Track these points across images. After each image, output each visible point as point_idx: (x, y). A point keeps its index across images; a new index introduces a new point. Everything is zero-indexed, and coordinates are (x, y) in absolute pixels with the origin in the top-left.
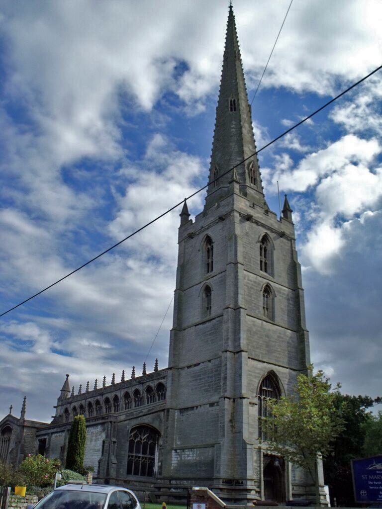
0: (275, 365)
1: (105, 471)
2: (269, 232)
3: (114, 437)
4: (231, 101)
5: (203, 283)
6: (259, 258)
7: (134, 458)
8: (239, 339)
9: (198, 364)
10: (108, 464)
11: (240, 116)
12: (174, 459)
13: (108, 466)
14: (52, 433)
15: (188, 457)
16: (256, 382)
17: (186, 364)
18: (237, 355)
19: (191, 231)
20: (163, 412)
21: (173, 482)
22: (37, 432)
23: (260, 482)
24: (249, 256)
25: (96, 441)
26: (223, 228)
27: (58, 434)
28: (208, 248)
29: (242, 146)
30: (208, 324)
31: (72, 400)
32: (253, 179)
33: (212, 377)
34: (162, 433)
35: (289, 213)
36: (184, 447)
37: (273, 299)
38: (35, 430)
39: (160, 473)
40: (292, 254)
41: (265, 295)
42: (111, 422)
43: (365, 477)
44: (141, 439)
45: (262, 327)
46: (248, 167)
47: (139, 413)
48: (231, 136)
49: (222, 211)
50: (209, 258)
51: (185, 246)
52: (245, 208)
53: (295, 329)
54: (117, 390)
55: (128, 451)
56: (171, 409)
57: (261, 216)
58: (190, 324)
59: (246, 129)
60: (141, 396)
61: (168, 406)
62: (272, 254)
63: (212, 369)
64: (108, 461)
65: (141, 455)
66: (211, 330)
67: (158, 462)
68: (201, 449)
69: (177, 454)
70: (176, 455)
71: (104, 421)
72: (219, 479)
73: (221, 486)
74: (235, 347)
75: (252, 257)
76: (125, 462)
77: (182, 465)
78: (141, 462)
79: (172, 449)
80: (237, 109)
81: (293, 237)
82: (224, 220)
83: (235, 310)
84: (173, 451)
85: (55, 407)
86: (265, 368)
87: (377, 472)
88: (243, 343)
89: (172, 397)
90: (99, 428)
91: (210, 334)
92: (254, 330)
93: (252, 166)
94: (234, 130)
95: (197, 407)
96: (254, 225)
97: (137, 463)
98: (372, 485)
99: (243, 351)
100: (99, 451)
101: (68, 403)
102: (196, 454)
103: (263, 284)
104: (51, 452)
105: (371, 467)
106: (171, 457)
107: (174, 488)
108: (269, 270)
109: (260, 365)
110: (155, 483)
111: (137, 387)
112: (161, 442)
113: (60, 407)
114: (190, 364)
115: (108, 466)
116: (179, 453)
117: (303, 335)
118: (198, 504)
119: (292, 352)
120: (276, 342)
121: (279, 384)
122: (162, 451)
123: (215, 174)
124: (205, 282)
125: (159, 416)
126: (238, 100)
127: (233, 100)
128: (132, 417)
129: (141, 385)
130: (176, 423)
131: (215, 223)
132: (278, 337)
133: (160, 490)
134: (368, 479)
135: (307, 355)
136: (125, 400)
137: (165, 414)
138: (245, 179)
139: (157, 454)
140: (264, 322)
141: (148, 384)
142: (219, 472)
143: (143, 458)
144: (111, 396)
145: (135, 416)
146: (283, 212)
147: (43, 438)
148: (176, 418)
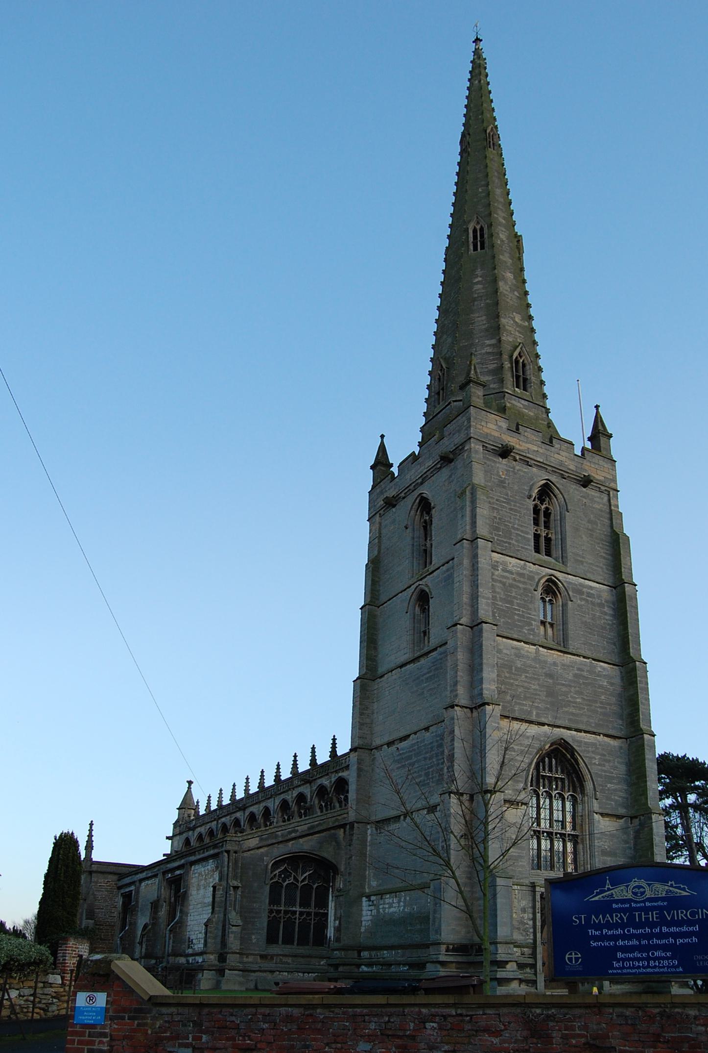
0: (569, 729)
1: (219, 939)
2: (554, 478)
3: (235, 877)
4: (475, 231)
5: (413, 587)
6: (532, 529)
7: (282, 915)
8: (481, 681)
9: (405, 738)
10: (224, 926)
11: (494, 257)
12: (367, 913)
13: (224, 930)
14: (141, 880)
15: (389, 908)
17: (386, 739)
19: (391, 493)
20: (342, 830)
21: (365, 954)
22: (119, 880)
24: (506, 525)
25: (205, 888)
26: (450, 476)
27: (149, 882)
28: (425, 522)
29: (498, 316)
30: (423, 661)
31: (196, 824)
32: (521, 379)
33: (430, 758)
34: (342, 868)
35: (603, 440)
36: (384, 889)
37: (564, 605)
38: (115, 877)
39: (338, 940)
40: (611, 519)
41: (547, 599)
42: (228, 852)
43: (580, 919)
44: (295, 878)
45: (537, 658)
46: (511, 356)
47: (290, 833)
48: (475, 300)
49: (447, 445)
50: (426, 540)
51: (380, 523)
52: (496, 434)
53: (615, 659)
54: (269, 798)
55: (267, 901)
56: (357, 823)
58: (392, 665)
59: (506, 283)
60: (308, 805)
61: (352, 816)
62: (562, 519)
63: (431, 743)
64: (224, 920)
65: (312, 910)
66: (428, 673)
67: (335, 920)
68: (412, 892)
69: (371, 903)
70: (370, 906)
71: (216, 851)
72: (439, 944)
73: (442, 958)
74: (472, 698)
75: (513, 528)
76: (263, 922)
77: (381, 922)
78: (297, 921)
79: (362, 895)
81: (612, 485)
82: (451, 461)
83: (472, 628)
84: (364, 899)
85: (168, 838)
86: (545, 735)
87: (614, 906)
88: (489, 688)
89: (358, 801)
90: (211, 865)
91: (427, 679)
93: (520, 354)
94: (480, 286)
96: (518, 466)
97: (289, 924)
98: (596, 938)
99: (488, 704)
100: (204, 905)
101: (190, 829)
102: (405, 902)
103: (539, 580)
104: (139, 913)
105: (598, 894)
106: (362, 910)
107: (365, 965)
108: (556, 551)
109: (533, 730)
110: (329, 958)
111: (301, 789)
112: (340, 883)
113: (178, 838)
114: (391, 739)
115: (224, 930)
116: (375, 902)
117: (634, 669)
118: (88, 994)
119: (610, 704)
120: (570, 686)
121: (578, 764)
122: (341, 899)
123: (439, 379)
124: (417, 584)
125: (334, 838)
126: (490, 226)
127: (478, 227)
128: (274, 841)
129: (308, 785)
130: (368, 848)
132: (575, 676)
133: (337, 969)
134: (589, 925)
135: (641, 707)
136: (283, 815)
137: (347, 832)
138: (502, 381)
139: (331, 905)
140: (541, 649)
141: (319, 782)
142: (438, 931)
143: (301, 913)
144: (257, 809)
145: (280, 839)
146: (589, 439)
147: (127, 890)
148: (369, 838)
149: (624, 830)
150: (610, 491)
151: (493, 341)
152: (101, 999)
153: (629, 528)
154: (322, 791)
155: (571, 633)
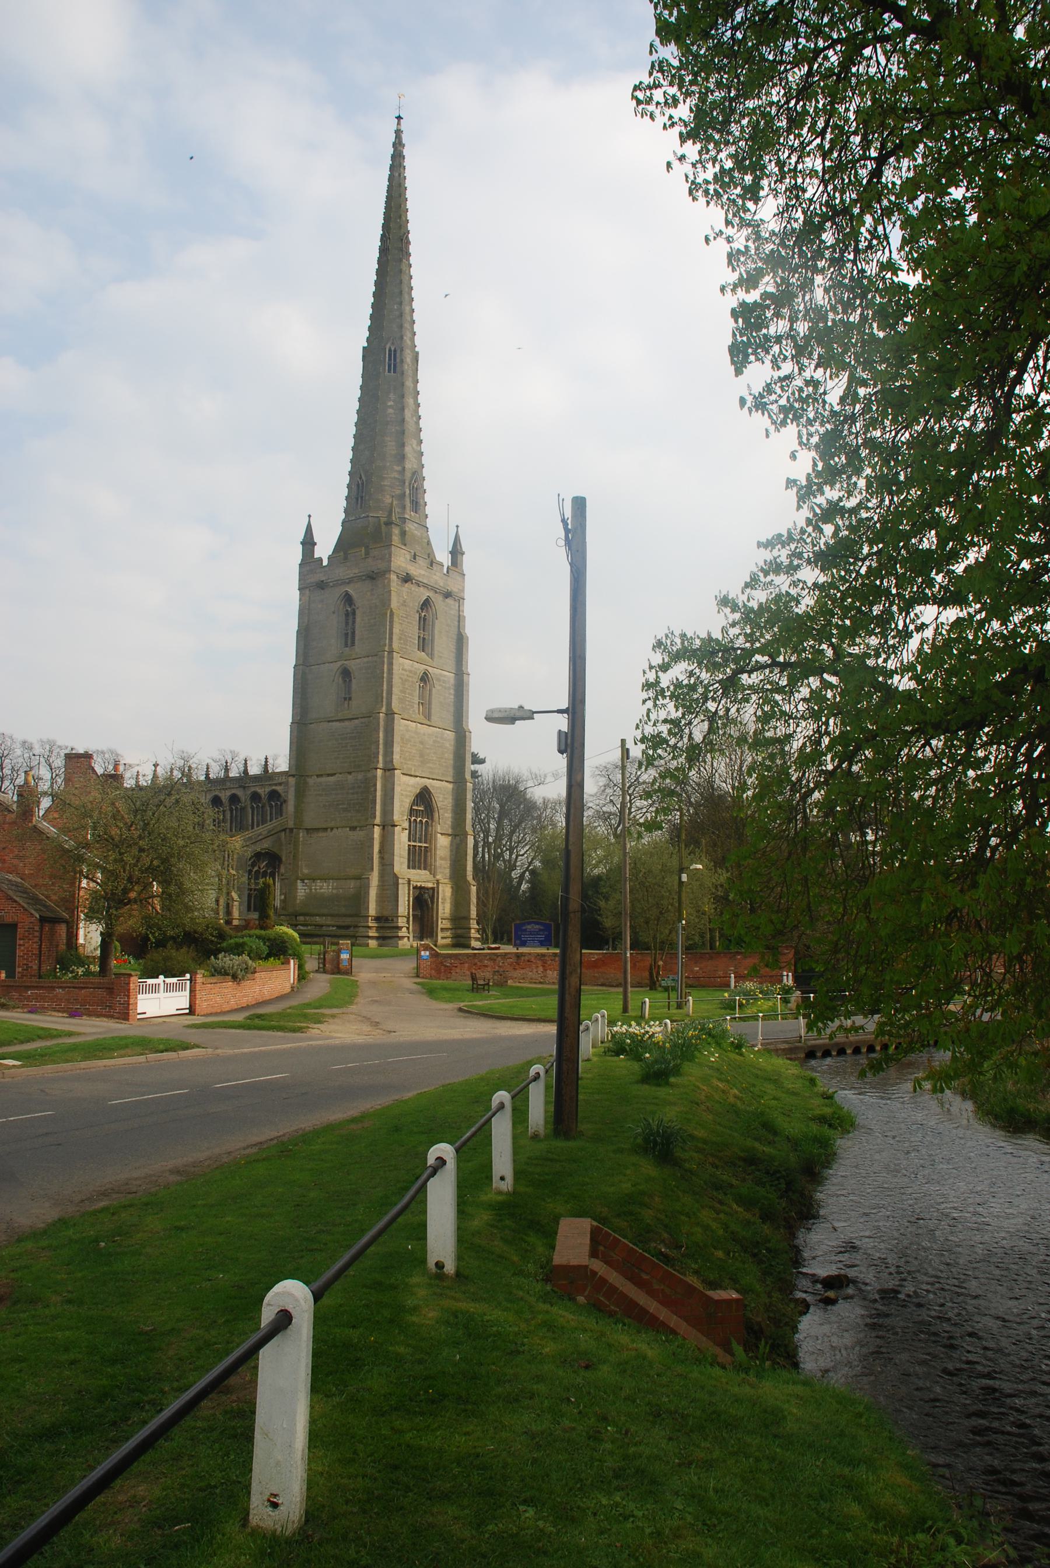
4: (390, 350)
8: (392, 753)
12: (301, 891)
16: (408, 802)
18: (388, 773)
21: (301, 918)
23: (408, 919)
30: (347, 723)
34: (284, 859)
35: (459, 556)
37: (430, 690)
39: (283, 908)
57: (423, 572)
80: (398, 369)
82: (374, 579)
92: (407, 737)
94: (390, 411)
95: (332, 829)
108: (428, 649)
109: (412, 780)
112: (282, 870)
126: (402, 350)
131: (359, 578)
149: (452, 842)
150: (460, 600)
151: (399, 468)
152: (428, 953)
153: (469, 630)
154: (255, 797)
155: (433, 711)
